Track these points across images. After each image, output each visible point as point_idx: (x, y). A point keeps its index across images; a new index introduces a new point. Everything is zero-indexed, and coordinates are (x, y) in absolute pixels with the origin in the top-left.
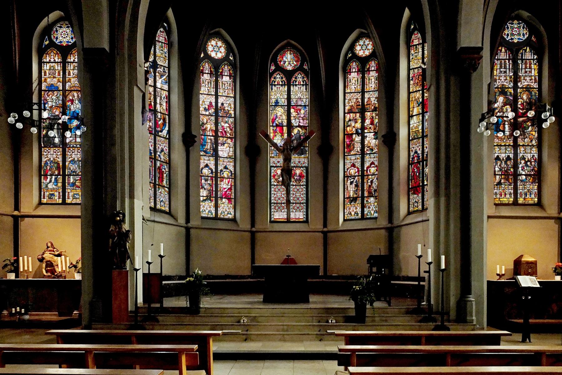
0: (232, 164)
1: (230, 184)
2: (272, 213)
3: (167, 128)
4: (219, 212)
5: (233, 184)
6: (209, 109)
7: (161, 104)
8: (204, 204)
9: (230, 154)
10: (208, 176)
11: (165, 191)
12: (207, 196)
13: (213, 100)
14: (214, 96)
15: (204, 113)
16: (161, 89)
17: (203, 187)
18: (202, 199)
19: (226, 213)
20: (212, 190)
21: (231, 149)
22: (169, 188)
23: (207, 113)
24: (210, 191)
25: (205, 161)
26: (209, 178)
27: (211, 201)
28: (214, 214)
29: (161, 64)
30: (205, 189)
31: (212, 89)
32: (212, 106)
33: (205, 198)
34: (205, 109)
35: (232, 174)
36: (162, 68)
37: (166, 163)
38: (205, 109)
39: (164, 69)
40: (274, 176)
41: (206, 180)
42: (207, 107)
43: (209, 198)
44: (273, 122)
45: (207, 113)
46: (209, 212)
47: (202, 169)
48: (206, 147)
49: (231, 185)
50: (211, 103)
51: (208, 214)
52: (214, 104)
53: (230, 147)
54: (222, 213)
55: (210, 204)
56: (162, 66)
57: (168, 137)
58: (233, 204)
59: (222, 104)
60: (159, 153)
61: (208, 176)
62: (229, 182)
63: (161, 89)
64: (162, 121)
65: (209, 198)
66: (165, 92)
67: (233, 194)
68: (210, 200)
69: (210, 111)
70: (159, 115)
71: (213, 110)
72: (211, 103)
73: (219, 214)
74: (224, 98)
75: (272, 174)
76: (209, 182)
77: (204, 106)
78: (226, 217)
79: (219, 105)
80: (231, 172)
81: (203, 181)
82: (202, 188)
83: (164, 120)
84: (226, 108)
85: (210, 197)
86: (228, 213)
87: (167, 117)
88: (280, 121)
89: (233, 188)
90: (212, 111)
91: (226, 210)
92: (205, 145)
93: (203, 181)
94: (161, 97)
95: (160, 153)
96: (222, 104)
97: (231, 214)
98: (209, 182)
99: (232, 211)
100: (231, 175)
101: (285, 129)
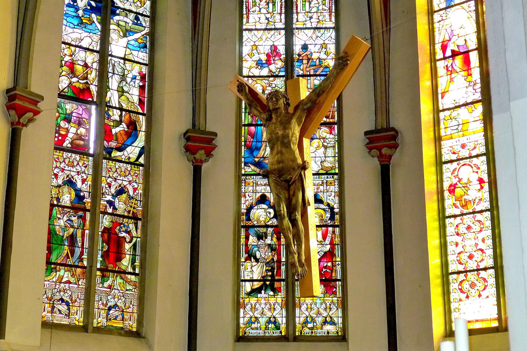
0: (335, 188)
1: (328, 241)
2: (453, 306)
3: (140, 141)
4: (299, 320)
5: (337, 240)
6: (268, 62)
7: (121, 92)
8: (253, 300)
9: (326, 164)
10: (267, 226)
11: (129, 282)
12: (263, 279)
13: (280, 40)
14: (283, 32)
15: (256, 72)
16: (124, 59)
17: (251, 256)
18: (248, 287)
19: (320, 320)
20: (279, 261)
21: (330, 152)
22: (142, 276)
23: (265, 72)
24: (273, 267)
25: (259, 188)
26: (270, 230)
27: (276, 291)
28: (283, 327)
29: (127, 6)
30: (257, 260)
31: (278, 17)
32: (278, 55)
33: (257, 285)
34: (259, 64)
35: (333, 214)
36: (132, 16)
37: (135, 218)
38: (259, 64)
39: (137, 18)
40: (452, 189)
41: (260, 237)
42: (264, 58)
43: (268, 284)
44: (444, 48)
45: (265, 72)
46: (269, 322)
47: (250, 209)
48: (261, 153)
49: (332, 243)
50: (274, 48)
51: (267, 328)
52: (282, 50)
53: (326, 147)
54: (306, 322)
55: (272, 300)
56: (130, 11)
57: (142, 160)
58: (339, 294)
59: (305, 47)
60: (109, 198)
61: (267, 226)
62: (324, 237)
63: (124, 59)
64: (123, 127)
65: (268, 284)
66: (137, 67)
67: (339, 268)
68: (274, 290)
69: (272, 67)
70: (115, 115)
71: (280, 64)
72: (274, 48)
73: (298, 326)
74: (310, 32)
75: (446, 185)
76: (268, 241)
77: (256, 57)
78: (319, 332)
79: (297, 49)
80: (332, 209)
81: (252, 240)
82: (248, 259)
83: (133, 126)
84: (315, 56)
85: (273, 280)
86: (325, 322)
87: (142, 119)
88: (461, 42)
89: (338, 251)
90: (277, 65)
91: (319, 313)
92: (258, 149)
93: (252, 240)
94: (123, 78)
95: (114, 196)
96: (305, 47)
97: (333, 323)
98: (268, 241)
99: (337, 314)
100: (332, 218)
101: (474, 57)
